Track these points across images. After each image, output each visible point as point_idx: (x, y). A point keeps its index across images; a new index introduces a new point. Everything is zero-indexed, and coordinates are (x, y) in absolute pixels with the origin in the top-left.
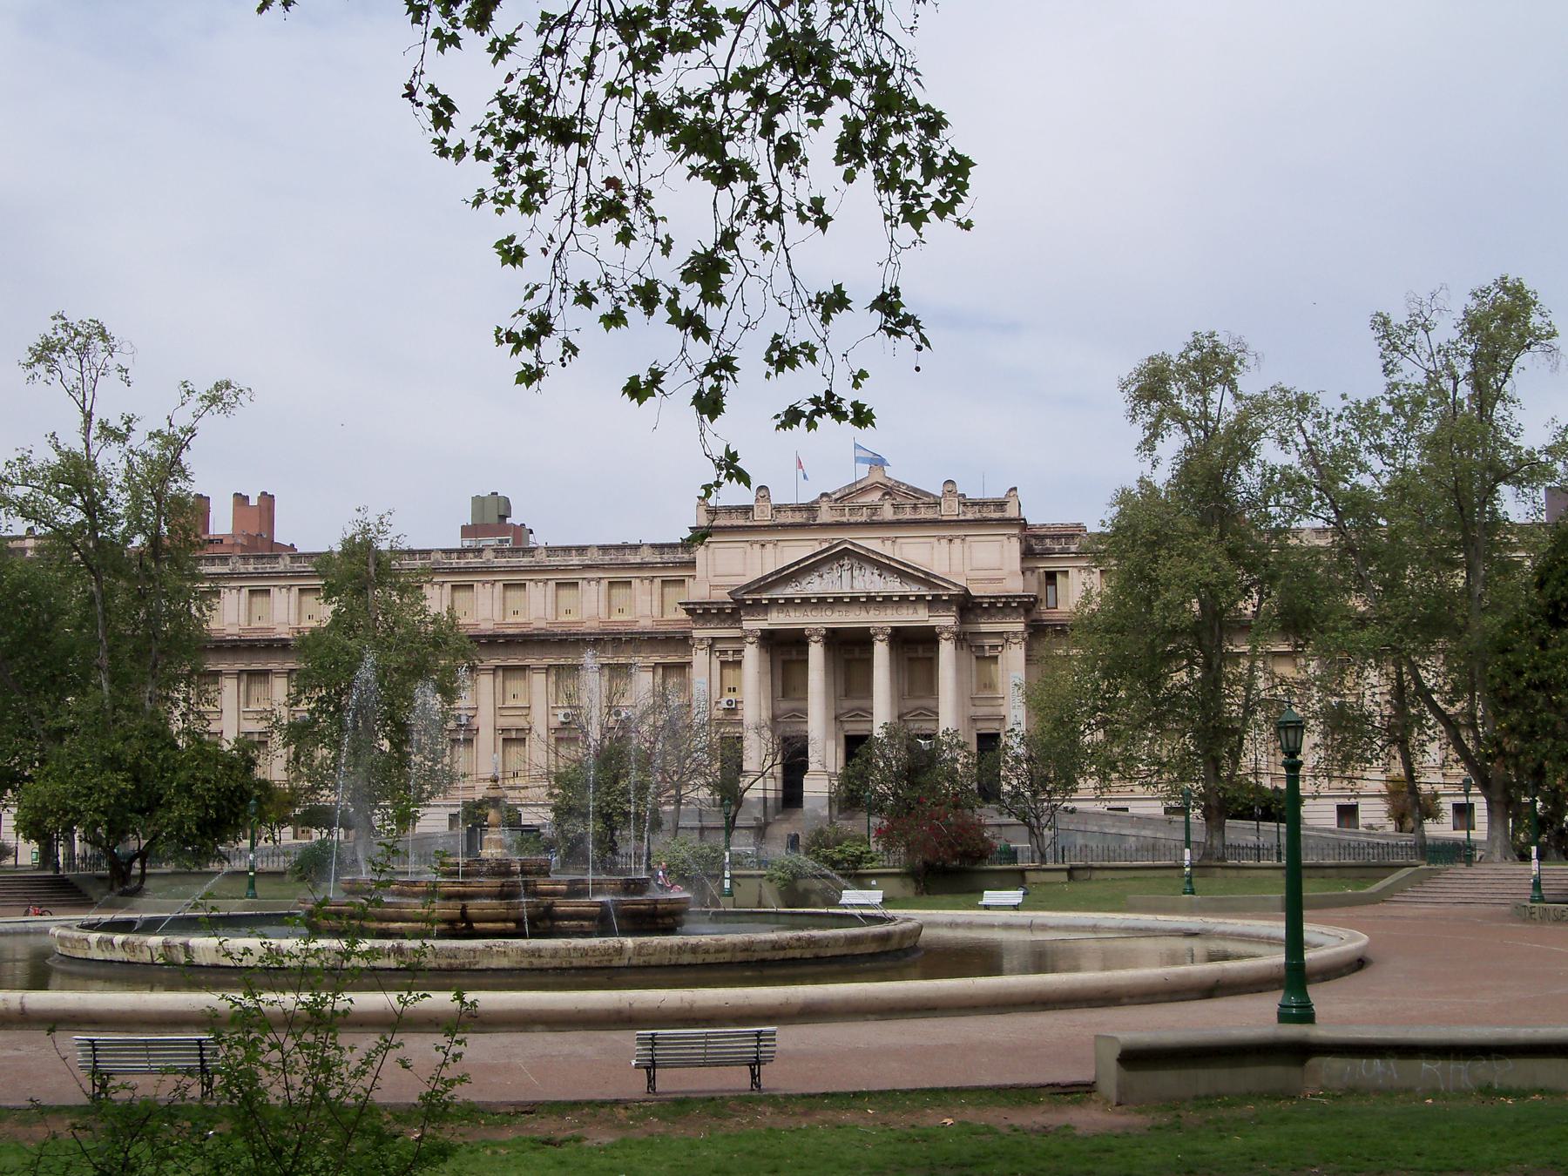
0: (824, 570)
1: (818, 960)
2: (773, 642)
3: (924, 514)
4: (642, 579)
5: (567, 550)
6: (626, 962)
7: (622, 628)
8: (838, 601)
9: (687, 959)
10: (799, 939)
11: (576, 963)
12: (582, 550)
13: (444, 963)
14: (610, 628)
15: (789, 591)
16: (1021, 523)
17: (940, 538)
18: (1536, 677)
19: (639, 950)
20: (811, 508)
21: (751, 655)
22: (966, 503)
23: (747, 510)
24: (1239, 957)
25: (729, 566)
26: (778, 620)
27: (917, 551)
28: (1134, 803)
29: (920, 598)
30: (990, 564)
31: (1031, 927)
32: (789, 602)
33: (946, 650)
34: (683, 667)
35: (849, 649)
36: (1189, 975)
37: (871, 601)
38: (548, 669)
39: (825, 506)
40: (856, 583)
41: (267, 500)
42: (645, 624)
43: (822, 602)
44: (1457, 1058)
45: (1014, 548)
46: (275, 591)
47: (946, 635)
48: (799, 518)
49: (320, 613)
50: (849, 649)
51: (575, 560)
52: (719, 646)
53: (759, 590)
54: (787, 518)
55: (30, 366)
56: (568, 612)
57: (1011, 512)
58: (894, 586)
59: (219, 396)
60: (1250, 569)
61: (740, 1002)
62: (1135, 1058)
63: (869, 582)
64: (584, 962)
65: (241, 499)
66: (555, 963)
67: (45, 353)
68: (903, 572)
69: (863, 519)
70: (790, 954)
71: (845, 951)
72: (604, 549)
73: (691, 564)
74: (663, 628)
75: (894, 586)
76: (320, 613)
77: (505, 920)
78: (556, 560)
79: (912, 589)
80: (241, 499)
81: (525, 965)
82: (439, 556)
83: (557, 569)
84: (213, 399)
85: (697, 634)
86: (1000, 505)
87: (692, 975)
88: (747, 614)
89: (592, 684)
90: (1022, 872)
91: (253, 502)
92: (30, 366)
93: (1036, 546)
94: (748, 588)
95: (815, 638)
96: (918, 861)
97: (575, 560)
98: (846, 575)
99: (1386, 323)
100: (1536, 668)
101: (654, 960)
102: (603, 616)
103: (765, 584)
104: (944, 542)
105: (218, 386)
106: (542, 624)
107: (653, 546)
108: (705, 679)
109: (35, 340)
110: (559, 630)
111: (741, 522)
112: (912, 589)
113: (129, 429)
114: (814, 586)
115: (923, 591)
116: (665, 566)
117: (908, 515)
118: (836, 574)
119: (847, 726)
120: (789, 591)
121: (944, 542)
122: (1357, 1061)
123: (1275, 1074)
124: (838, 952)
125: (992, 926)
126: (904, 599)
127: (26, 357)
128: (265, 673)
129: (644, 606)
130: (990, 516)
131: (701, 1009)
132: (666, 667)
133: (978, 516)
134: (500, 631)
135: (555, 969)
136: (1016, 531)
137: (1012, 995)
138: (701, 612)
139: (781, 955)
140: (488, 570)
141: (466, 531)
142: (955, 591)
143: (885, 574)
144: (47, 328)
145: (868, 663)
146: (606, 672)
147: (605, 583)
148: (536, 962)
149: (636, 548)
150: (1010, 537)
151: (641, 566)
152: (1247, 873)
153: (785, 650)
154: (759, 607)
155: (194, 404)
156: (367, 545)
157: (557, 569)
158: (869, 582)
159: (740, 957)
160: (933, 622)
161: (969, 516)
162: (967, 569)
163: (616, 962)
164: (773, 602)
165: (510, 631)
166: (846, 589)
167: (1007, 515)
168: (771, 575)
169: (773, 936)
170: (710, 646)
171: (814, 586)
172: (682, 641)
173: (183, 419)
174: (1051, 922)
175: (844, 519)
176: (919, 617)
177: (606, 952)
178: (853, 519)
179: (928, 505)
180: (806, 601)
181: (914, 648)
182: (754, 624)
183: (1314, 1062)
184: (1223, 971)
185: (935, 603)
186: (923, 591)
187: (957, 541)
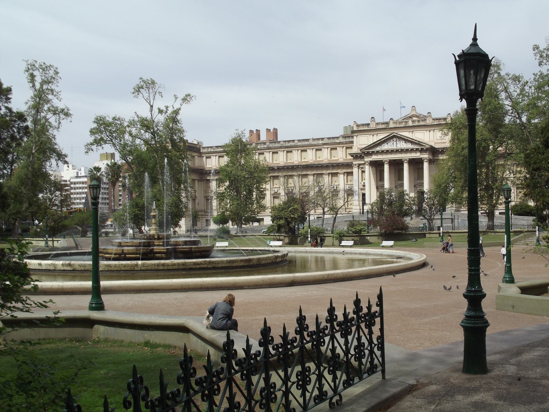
0: (388, 141)
1: (214, 268)
3: (422, 123)
5: (318, 139)
6: (139, 269)
7: (335, 162)
9: (161, 268)
10: (205, 261)
11: (123, 269)
12: (322, 139)
13: (83, 268)
14: (331, 162)
15: (378, 149)
18: (535, 166)
19: (143, 265)
20: (387, 123)
21: (367, 168)
22: (395, 123)
23: (368, 125)
25: (362, 142)
26: (375, 158)
29: (417, 149)
32: (378, 152)
33: (426, 165)
34: (351, 173)
35: (396, 165)
36: (275, 278)
37: (402, 151)
38: (329, 174)
39: (391, 122)
41: (275, 130)
42: (296, 163)
43: (387, 152)
44: (138, 329)
46: (338, 148)
48: (383, 126)
49: (225, 160)
50: (396, 165)
51: (321, 142)
52: (361, 166)
53: (369, 149)
55: (133, 93)
56: (319, 158)
58: (409, 146)
59: (186, 99)
61: (79, 286)
64: (126, 269)
65: (268, 130)
66: (116, 269)
67: (138, 90)
68: (412, 142)
70: (202, 266)
71: (228, 265)
72: (329, 138)
73: (352, 142)
74: (346, 161)
75: (409, 146)
76: (225, 160)
77: (136, 254)
78: (315, 143)
80: (268, 130)
81: (106, 269)
82: (282, 143)
83: (315, 145)
84: (184, 100)
85: (354, 163)
87: (143, 274)
89: (326, 180)
90: (425, 234)
91: (272, 131)
92: (133, 93)
94: (365, 148)
96: (383, 231)
97: (321, 142)
99: (538, 48)
100: (535, 163)
101: (149, 268)
105: (187, 96)
106: (312, 162)
107: (328, 138)
108: (357, 176)
109: (134, 85)
110: (317, 163)
111: (366, 128)
113: (167, 110)
114: (385, 147)
116: (346, 144)
117: (417, 124)
119: (399, 189)
120: (378, 149)
121: (428, 132)
123: (78, 331)
124: (224, 265)
125: (356, 254)
126: (412, 150)
127: (133, 91)
128: (337, 173)
129: (341, 155)
131: (66, 289)
133: (438, 123)
134: (300, 164)
135: (116, 271)
137: (189, 285)
138: (356, 156)
139: (198, 266)
140: (296, 146)
142: (427, 147)
144: (138, 82)
145: (422, 168)
148: (110, 269)
151: (339, 143)
152: (497, 234)
153: (378, 166)
154: (369, 154)
155: (179, 101)
156: (240, 140)
159: (181, 267)
160: (422, 156)
161: (435, 123)
162: (435, 139)
163: (136, 269)
164: (373, 152)
165: (303, 164)
169: (228, 259)
170: (358, 166)
171: (385, 147)
172: (349, 165)
173: (177, 106)
174: (371, 252)
175: (397, 126)
176: (417, 155)
177: (132, 265)
178: (400, 126)
179: (423, 121)
181: (416, 164)
182: (368, 159)
183: (96, 326)
184: (203, 282)
185: (422, 151)
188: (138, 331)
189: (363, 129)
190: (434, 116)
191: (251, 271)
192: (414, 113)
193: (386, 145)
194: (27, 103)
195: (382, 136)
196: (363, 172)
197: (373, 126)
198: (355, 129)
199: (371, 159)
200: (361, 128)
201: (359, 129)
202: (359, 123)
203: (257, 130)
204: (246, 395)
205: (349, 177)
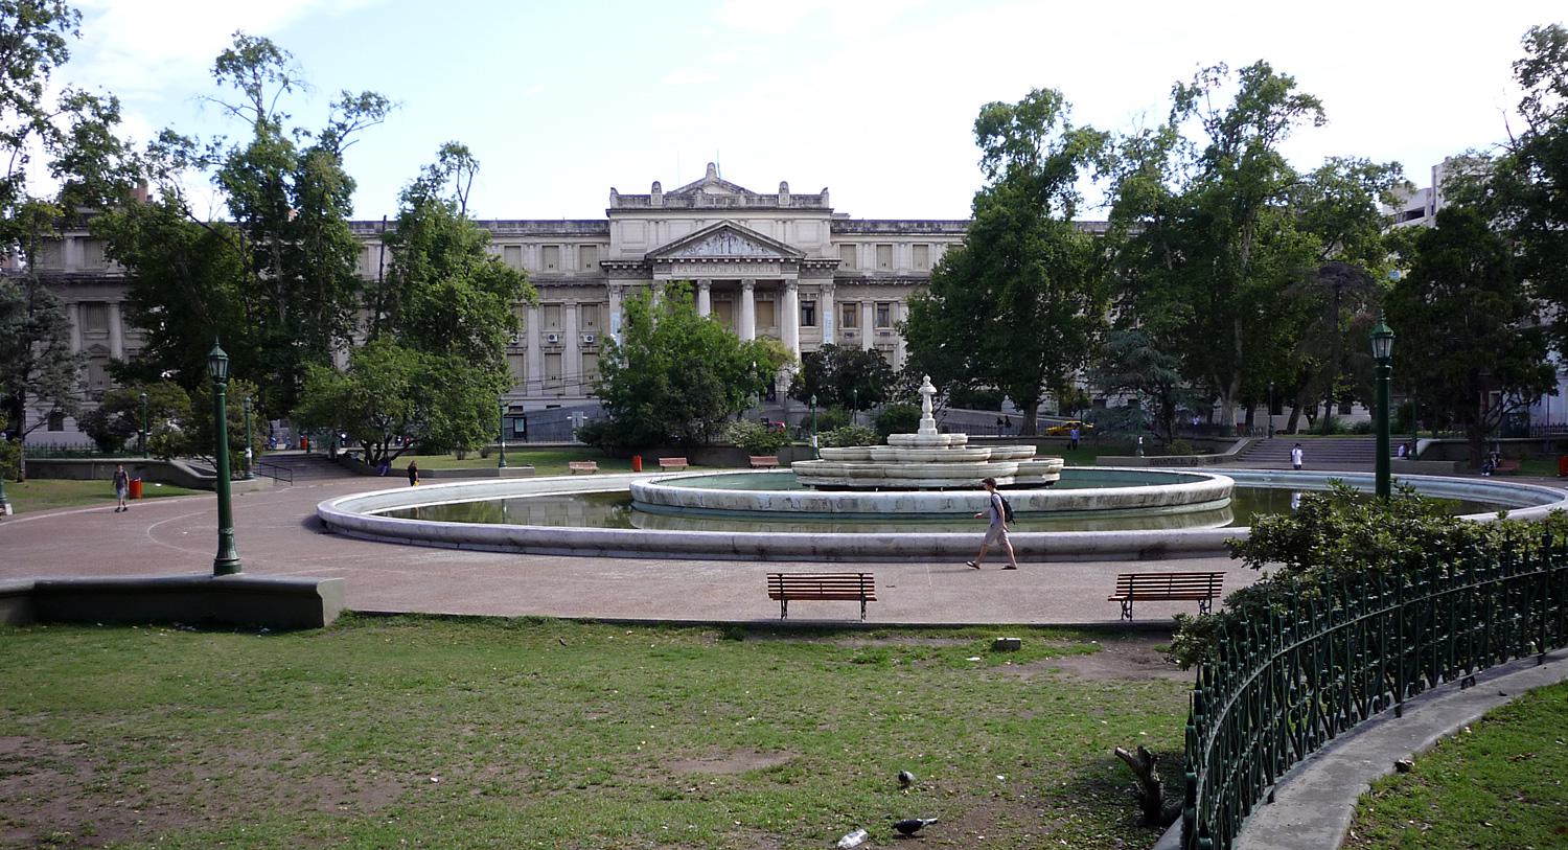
0: (710, 240)
2: (673, 288)
4: (528, 245)
5: (512, 223)
15: (678, 255)
16: (830, 211)
23: (647, 197)
24: (1226, 526)
25: (634, 238)
26: (678, 273)
27: (760, 225)
28: (526, 403)
29: (776, 260)
30: (807, 236)
31: (1507, 487)
32: (688, 261)
33: (793, 300)
48: (682, 204)
54: (674, 204)
58: (758, 252)
62: (548, 407)
63: (740, 249)
68: (764, 242)
69: (726, 206)
73: (607, 234)
75: (758, 252)
82: (570, 225)
86: (818, 199)
88: (658, 270)
93: (842, 226)
94: (659, 252)
95: (749, 286)
102: (83, 266)
103: (682, 244)
104: (652, 223)
107: (536, 222)
111: (642, 206)
114: (704, 251)
115: (778, 256)
116: (583, 235)
126: (765, 260)
128: (103, 305)
129: (569, 262)
130: (814, 205)
132: (584, 305)
136: (828, 217)
141: (608, 212)
146: (580, 307)
147: (539, 247)
149: (562, 222)
157: (506, 236)
158: (740, 249)
161: (797, 206)
164: (676, 261)
166: (726, 253)
168: (675, 243)
171: (704, 251)
175: (713, 206)
176: (773, 273)
178: (719, 206)
181: (769, 293)
185: (786, 264)
186: (778, 256)
187: (789, 223)
188: (1151, 563)
189: (632, 207)
190: (793, 191)
191: (429, 547)
192: (712, 178)
193: (705, 246)
194: (423, 169)
195: (681, 227)
197: (656, 203)
199: (669, 277)
201: (624, 206)
203: (57, 174)
204: (1321, 722)
205: (552, 318)
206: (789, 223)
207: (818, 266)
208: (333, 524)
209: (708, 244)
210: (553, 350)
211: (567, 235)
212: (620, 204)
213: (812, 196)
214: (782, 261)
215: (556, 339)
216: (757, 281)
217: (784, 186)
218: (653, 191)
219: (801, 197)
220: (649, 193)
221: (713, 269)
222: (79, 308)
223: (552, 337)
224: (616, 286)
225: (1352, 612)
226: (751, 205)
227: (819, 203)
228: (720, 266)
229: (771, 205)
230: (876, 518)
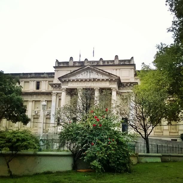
0: (83, 73)
4: (44, 81)
8: (86, 80)
17: (113, 69)
21: (64, 94)
23: (67, 63)
26: (71, 85)
32: (73, 80)
33: (114, 93)
37: (94, 80)
39: (86, 62)
40: (91, 76)
45: (133, 73)
47: (114, 90)
57: (132, 63)
58: (100, 77)
60: (168, 179)
62: (172, 140)
69: (95, 65)
79: (105, 78)
85: (53, 92)
86: (129, 61)
98: (89, 74)
108: (55, 103)
112: (105, 78)
115: (107, 78)
118: (86, 74)
122: (156, 161)
126: (103, 80)
128: (39, 101)
143: (98, 74)
150: (131, 69)
160: (110, 86)
166: (88, 77)
167: (131, 63)
171: (80, 76)
176: (106, 85)
180: (77, 80)
185: (111, 81)
187: (118, 70)
190: (120, 58)
196: (60, 99)
198: (57, 65)
199: (67, 87)
200: (62, 65)
202: (59, 61)
206: (118, 70)
207: (128, 85)
208: (62, 172)
209: (82, 75)
210: (36, 117)
211: (44, 77)
212: (103, 63)
213: (127, 60)
214: (110, 80)
215: (37, 113)
216: (100, 88)
217: (117, 57)
218: (70, 60)
219: (122, 61)
220: (69, 61)
221: (84, 84)
222: (32, 102)
223: (35, 112)
224: (54, 93)
225: (122, 160)
226: (104, 64)
227: (130, 62)
228: (86, 83)
229: (111, 64)
230: (172, 137)
